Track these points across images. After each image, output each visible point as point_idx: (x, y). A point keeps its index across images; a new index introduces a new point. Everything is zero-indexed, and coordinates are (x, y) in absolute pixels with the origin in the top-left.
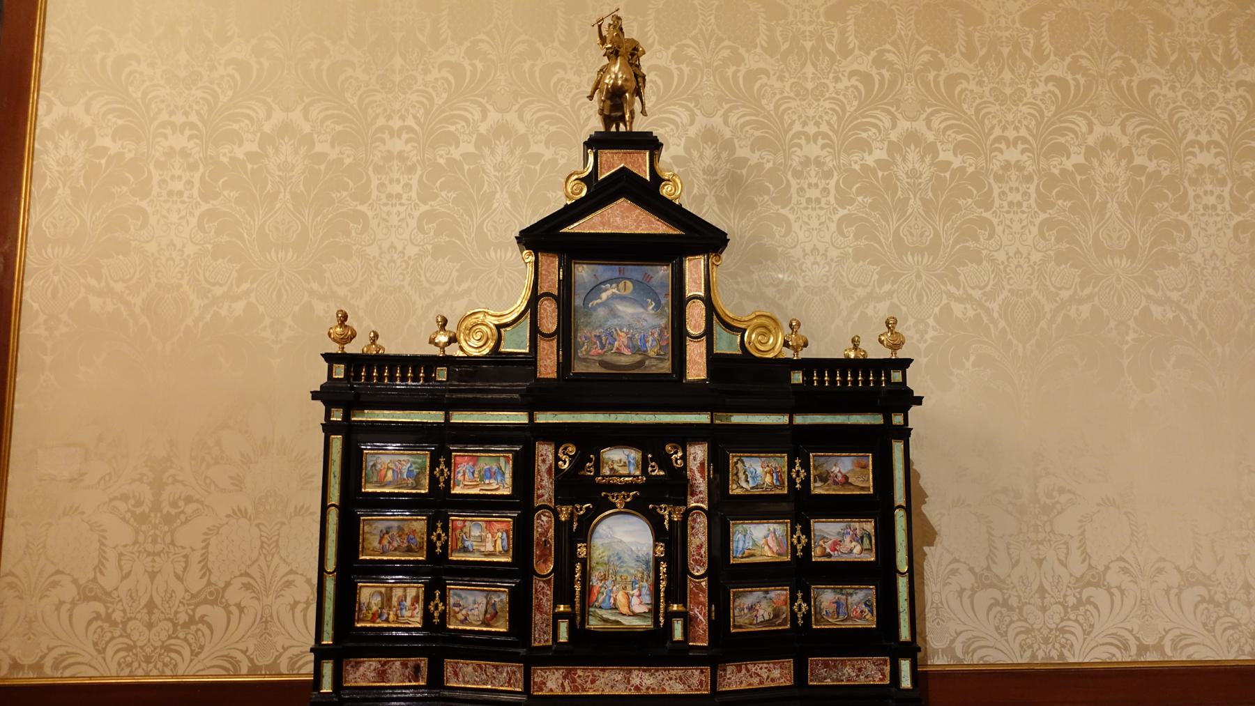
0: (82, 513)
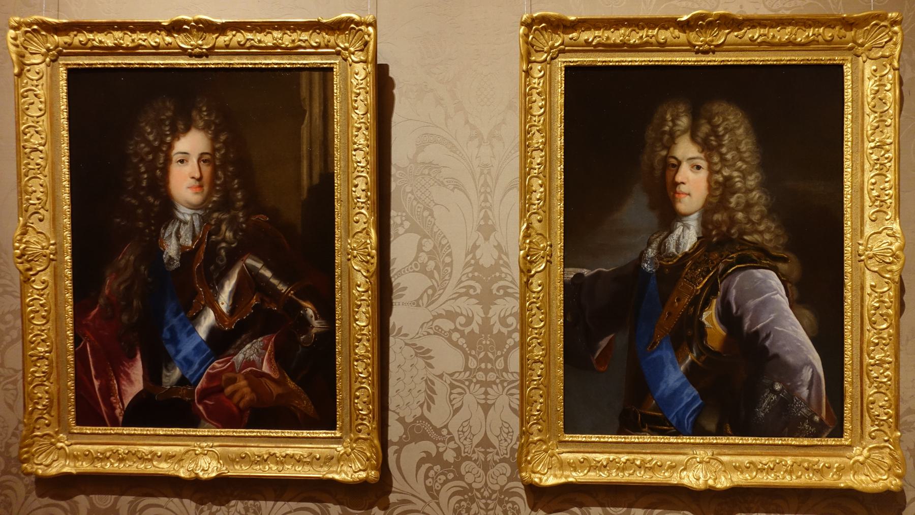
0: (406, 335)
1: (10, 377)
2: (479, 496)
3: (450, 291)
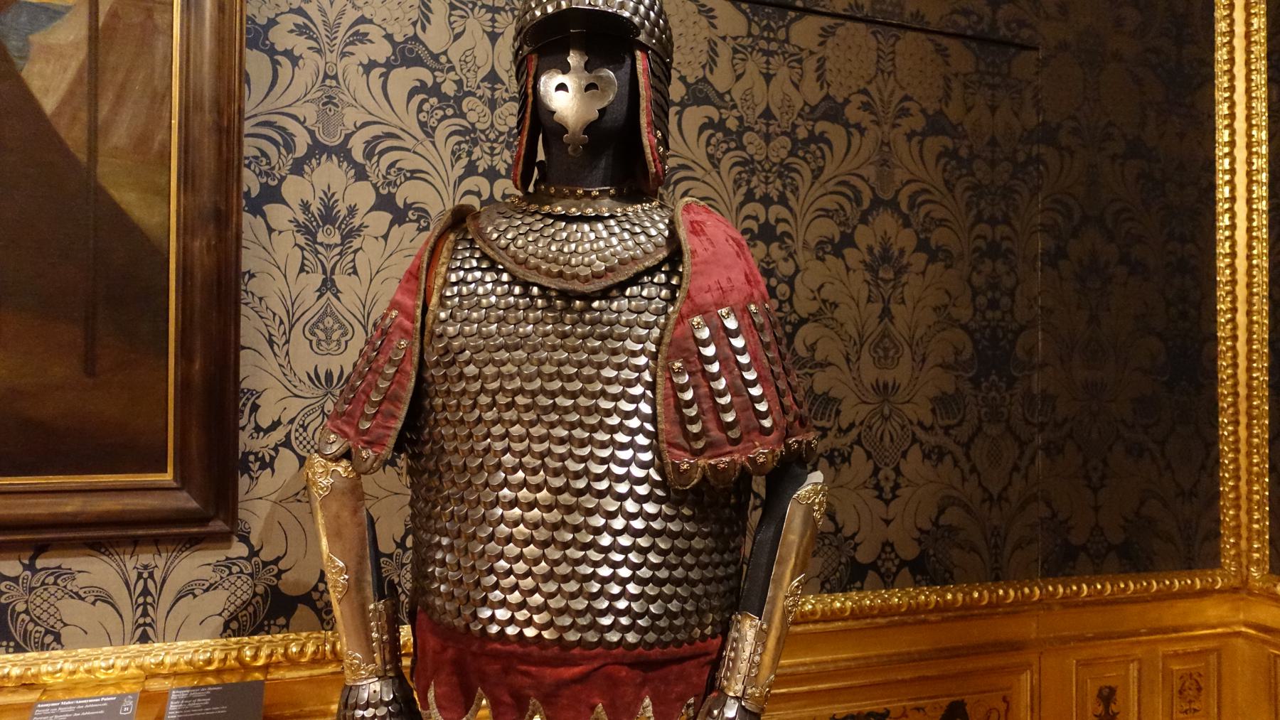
2: (483, 137)
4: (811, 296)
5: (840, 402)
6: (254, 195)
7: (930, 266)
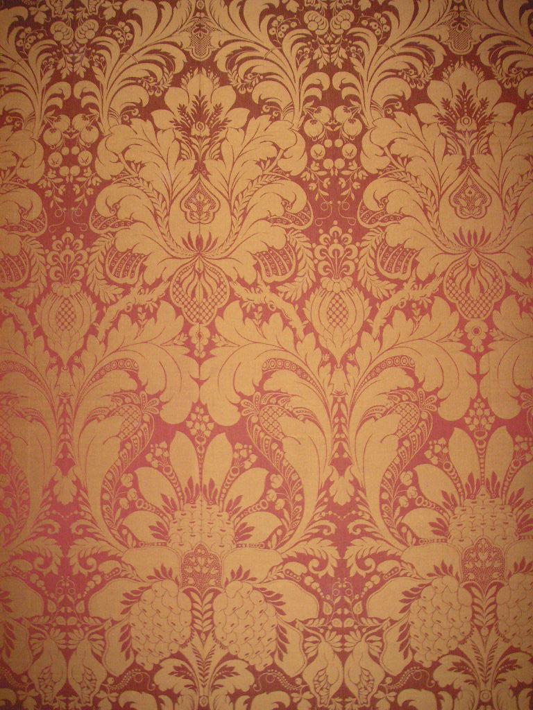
0: (254, 579)
1: (96, 627)
3: (27, 532)
4: (381, 152)
5: (146, 257)
6: (144, 105)
7: (519, 114)
